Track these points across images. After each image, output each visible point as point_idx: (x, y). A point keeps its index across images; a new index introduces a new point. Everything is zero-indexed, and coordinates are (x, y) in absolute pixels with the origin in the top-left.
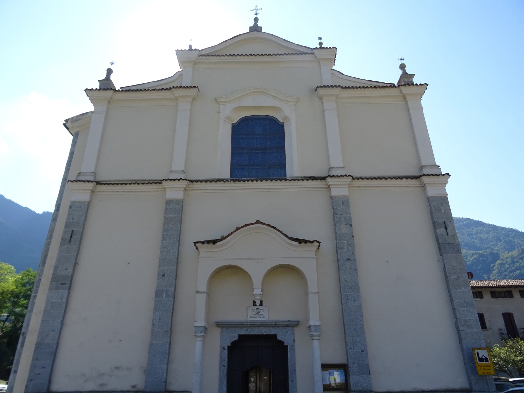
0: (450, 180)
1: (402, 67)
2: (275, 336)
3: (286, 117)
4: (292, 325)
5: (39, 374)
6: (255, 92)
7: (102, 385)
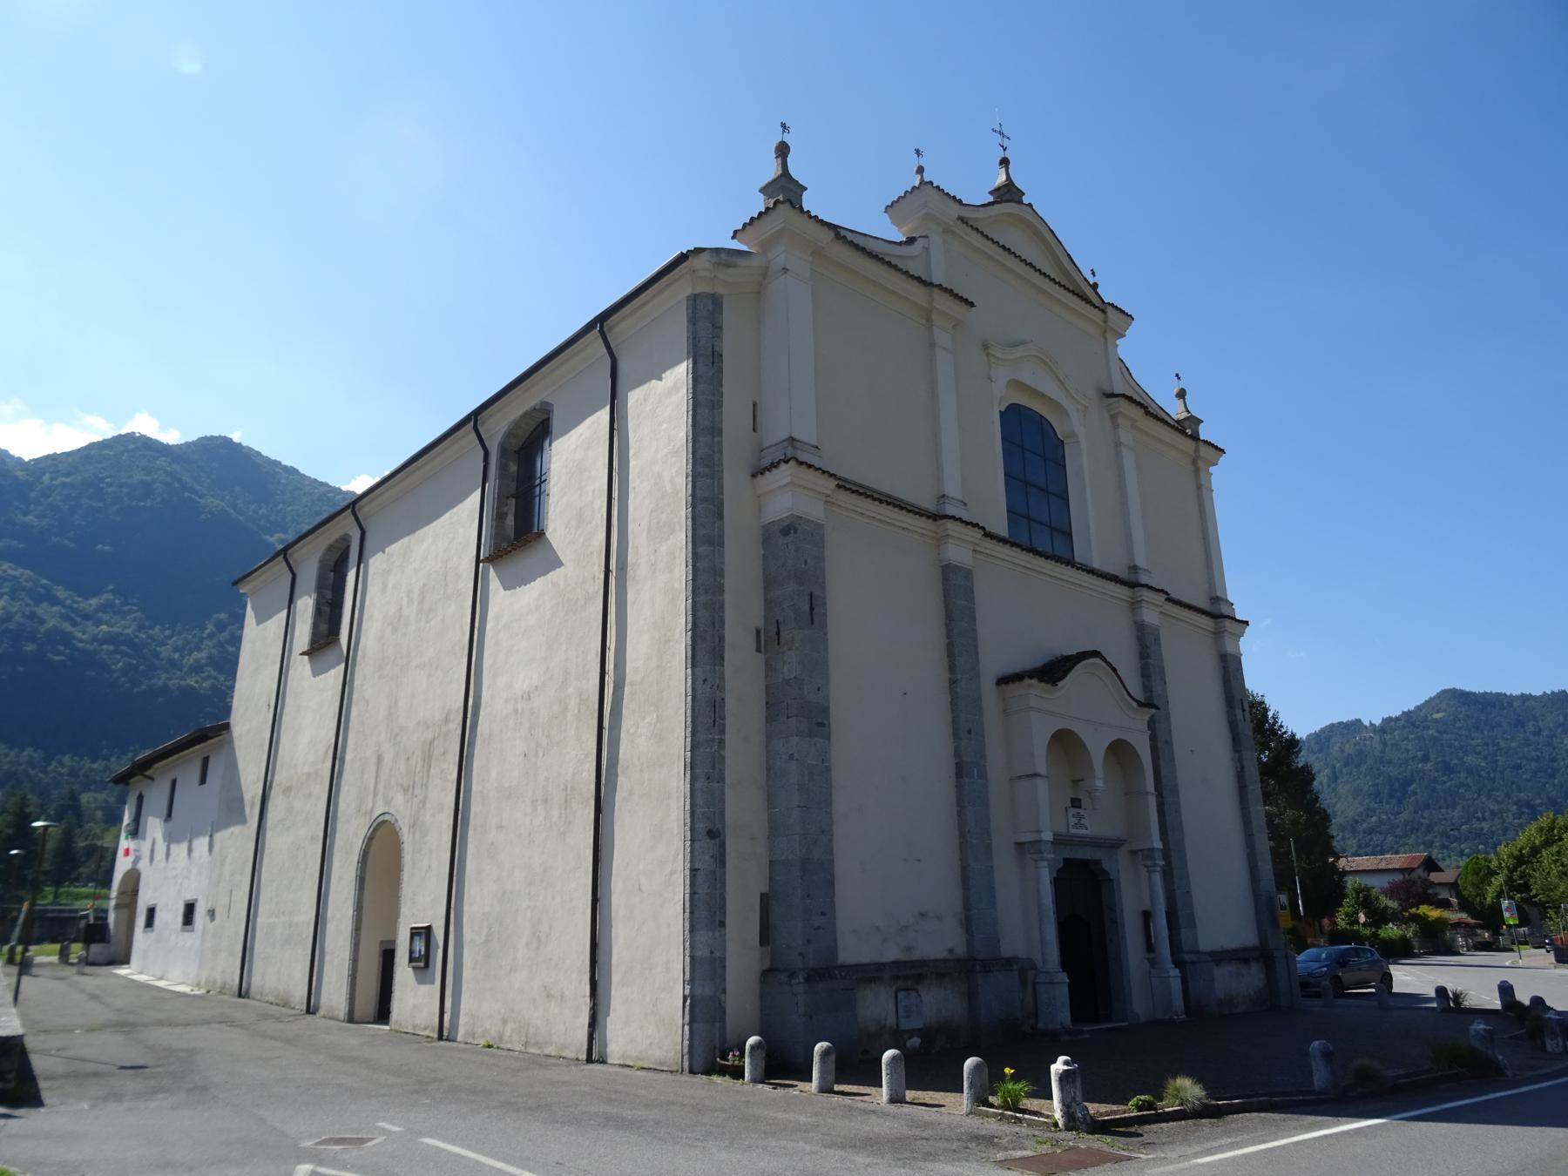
0: (1248, 630)
1: (783, 150)
2: (1098, 862)
3: (1073, 435)
4: (1113, 845)
5: (819, 928)
6: (1041, 359)
7: (908, 949)
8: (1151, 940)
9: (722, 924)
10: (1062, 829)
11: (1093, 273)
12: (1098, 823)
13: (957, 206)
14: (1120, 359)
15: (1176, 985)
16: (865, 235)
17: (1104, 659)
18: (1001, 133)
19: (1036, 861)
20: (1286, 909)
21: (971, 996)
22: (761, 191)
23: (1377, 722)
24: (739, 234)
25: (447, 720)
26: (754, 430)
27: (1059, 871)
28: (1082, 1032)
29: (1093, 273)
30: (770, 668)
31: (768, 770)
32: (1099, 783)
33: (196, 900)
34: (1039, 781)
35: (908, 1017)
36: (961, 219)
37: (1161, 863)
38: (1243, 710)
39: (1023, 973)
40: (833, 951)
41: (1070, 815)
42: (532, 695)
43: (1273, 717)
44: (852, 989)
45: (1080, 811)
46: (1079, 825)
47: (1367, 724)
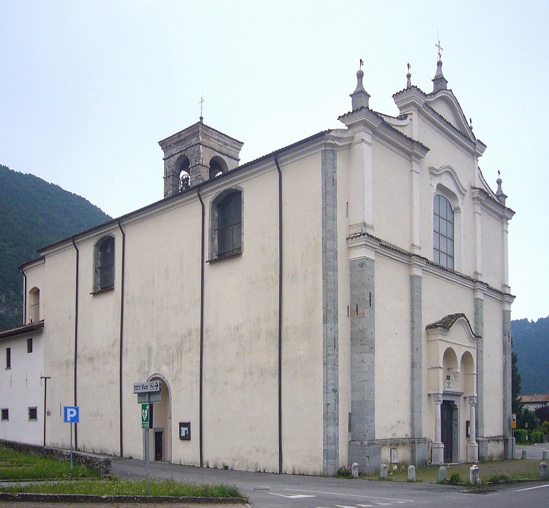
0: (515, 300)
4: (458, 395)
7: (394, 434)
8: (468, 433)
9: (338, 424)
12: (455, 387)
14: (479, 168)
15: (476, 449)
16: (390, 117)
17: (465, 317)
18: (439, 47)
19: (436, 401)
21: (413, 452)
23: (535, 320)
24: (341, 118)
26: (347, 216)
28: (447, 465)
30: (353, 324)
31: (352, 366)
32: (459, 370)
33: (37, 407)
35: (394, 458)
38: (509, 337)
41: (446, 383)
42: (239, 328)
44: (380, 448)
45: (449, 380)
47: (530, 321)
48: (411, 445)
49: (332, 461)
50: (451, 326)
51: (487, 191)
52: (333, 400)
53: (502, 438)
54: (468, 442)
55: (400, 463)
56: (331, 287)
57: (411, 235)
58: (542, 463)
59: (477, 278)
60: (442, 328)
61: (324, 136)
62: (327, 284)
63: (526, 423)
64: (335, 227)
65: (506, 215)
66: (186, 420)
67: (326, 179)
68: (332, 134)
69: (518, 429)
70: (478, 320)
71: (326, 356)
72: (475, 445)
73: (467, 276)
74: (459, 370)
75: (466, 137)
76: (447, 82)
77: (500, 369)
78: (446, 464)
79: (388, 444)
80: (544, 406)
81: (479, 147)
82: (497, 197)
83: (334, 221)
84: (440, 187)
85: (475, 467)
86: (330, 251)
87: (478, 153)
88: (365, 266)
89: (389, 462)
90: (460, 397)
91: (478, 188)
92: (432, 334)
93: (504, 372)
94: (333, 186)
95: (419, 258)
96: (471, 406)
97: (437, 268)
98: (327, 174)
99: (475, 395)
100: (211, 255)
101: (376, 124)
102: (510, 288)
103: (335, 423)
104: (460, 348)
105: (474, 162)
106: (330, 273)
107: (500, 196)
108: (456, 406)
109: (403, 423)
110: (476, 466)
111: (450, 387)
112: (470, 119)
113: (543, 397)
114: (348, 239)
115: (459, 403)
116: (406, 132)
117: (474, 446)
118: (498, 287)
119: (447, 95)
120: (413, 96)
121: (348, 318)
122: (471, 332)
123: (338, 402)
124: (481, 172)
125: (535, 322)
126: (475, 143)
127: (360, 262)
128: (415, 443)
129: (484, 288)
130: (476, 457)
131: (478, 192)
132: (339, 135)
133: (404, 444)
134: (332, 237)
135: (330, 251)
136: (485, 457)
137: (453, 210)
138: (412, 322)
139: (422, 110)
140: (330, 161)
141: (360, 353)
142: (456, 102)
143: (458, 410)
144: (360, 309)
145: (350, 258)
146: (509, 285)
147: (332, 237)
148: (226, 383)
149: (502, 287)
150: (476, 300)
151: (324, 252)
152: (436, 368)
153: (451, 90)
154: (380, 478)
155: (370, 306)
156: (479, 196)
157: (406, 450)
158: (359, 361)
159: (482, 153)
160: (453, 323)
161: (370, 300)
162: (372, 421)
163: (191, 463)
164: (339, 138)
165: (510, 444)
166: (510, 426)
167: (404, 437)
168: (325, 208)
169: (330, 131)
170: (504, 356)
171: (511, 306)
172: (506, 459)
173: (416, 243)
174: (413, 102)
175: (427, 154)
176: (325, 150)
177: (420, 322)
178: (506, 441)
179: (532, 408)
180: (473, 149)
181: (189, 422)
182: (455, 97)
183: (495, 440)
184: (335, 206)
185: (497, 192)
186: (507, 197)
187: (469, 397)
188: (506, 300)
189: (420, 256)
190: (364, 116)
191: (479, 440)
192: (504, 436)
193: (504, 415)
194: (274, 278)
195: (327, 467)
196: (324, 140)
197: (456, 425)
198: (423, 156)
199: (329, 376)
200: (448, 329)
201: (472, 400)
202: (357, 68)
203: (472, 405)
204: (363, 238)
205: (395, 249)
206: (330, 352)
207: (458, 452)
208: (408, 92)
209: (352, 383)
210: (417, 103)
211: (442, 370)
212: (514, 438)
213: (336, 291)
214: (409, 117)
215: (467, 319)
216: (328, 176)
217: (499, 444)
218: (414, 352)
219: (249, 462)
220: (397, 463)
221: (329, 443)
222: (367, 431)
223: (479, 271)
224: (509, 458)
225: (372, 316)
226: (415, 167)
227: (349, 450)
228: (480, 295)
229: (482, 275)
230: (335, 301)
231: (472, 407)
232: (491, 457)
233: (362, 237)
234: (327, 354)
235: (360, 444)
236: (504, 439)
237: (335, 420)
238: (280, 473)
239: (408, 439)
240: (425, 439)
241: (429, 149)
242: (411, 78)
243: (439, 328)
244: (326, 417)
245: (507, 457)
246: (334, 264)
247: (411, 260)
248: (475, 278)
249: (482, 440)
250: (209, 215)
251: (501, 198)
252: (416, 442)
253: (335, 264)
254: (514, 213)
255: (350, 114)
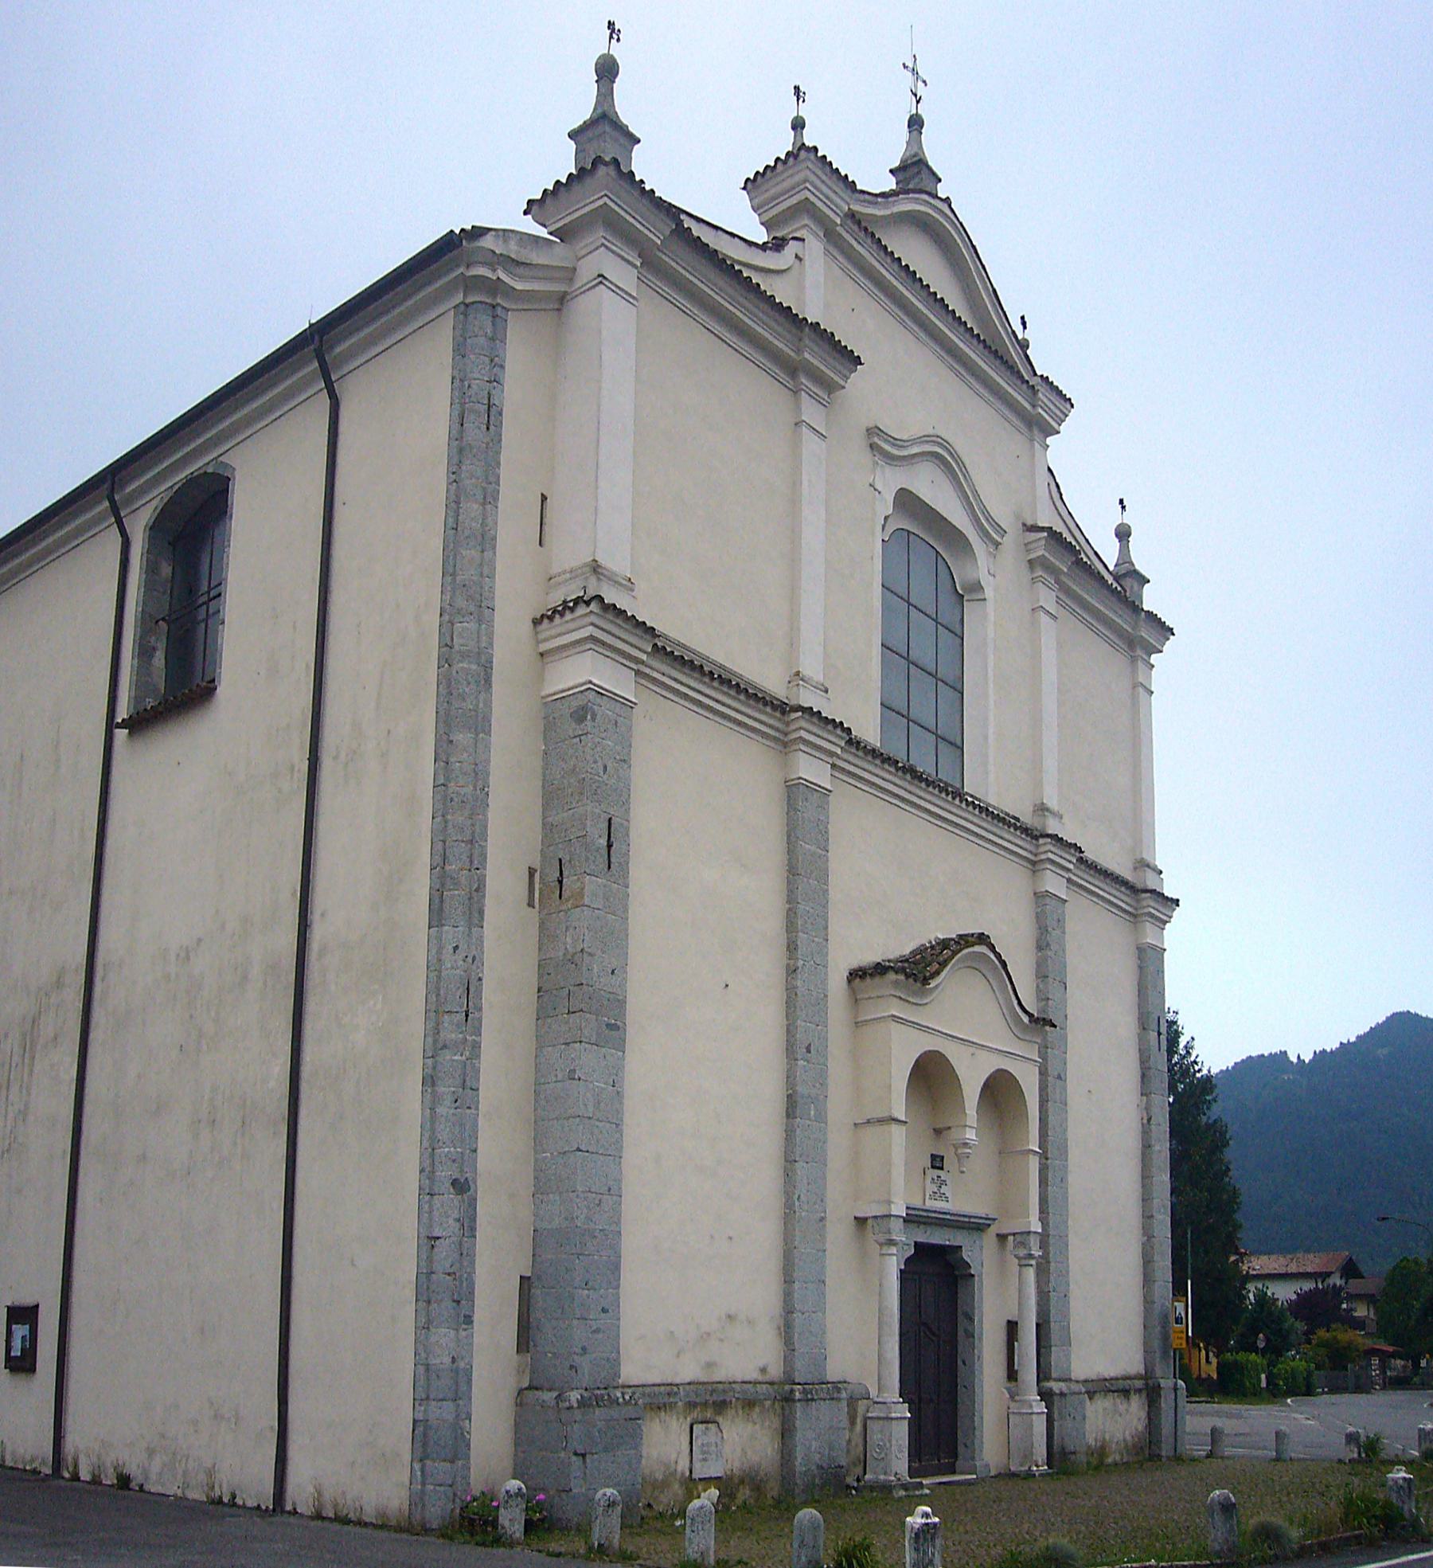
0: (1177, 913)
4: (977, 1226)
7: (710, 1365)
9: (468, 1320)
10: (917, 1202)
11: (1024, 324)
13: (846, 194)
14: (1049, 470)
15: (1040, 1426)
16: (717, 228)
17: (992, 948)
19: (881, 1245)
20: (1182, 1323)
21: (786, 1432)
22: (572, 135)
23: (1307, 1057)
24: (535, 208)
25: (59, 984)
26: (540, 544)
27: (908, 1261)
29: (1024, 324)
30: (546, 934)
32: (971, 1135)
34: (895, 1129)
35: (705, 1460)
36: (852, 215)
37: (1037, 1253)
39: (852, 1402)
40: (615, 1363)
41: (929, 1180)
42: (192, 955)
43: (1186, 1047)
45: (940, 1172)
46: (939, 1195)
48: (779, 1411)
49: (440, 1469)
50: (937, 973)
51: (1074, 543)
52: (451, 1221)
53: (1139, 1384)
54: (1012, 1397)
55: (730, 1478)
56: (463, 791)
57: (793, 644)
58: (1217, 1492)
59: (1044, 825)
60: (902, 977)
61: (460, 249)
62: (447, 778)
63: (1261, 1335)
64: (486, 571)
65: (1143, 635)
66: (27, 1300)
67: (463, 404)
68: (487, 242)
69: (1237, 1353)
70: (1048, 970)
71: (435, 1048)
72: (1036, 1410)
73: (1008, 815)
74: (971, 1135)
75: (1002, 358)
76: (940, 180)
77: (1131, 1141)
78: (918, 1480)
79: (680, 1404)
80: (1320, 1287)
81: (1045, 400)
82: (1117, 578)
83: (483, 551)
84: (906, 501)
85: (926, 1515)
86: (464, 656)
87: (1051, 426)
88: (593, 719)
89: (683, 1474)
90: (985, 1237)
91: (1042, 529)
92: (870, 998)
93: (1143, 1154)
94: (488, 429)
95: (815, 720)
96: (1020, 1266)
97: (892, 770)
98: (469, 386)
99: (1033, 1229)
100: (137, 699)
101: (656, 233)
102: (1161, 872)
103: (458, 1315)
104: (973, 1054)
105: (1033, 446)
106: (462, 737)
107: (1125, 575)
108: (970, 1267)
109: (750, 1322)
110: (928, 1510)
111: (943, 1197)
112: (1023, 318)
113: (1317, 1261)
114: (536, 622)
115: (980, 1255)
116: (781, 291)
117: (1032, 1414)
118: (1118, 864)
119: (930, 211)
120: (805, 181)
121: (531, 909)
122: (1015, 1002)
123: (473, 1229)
124: (1058, 486)
125: (1307, 1061)
126: (1033, 386)
127: (575, 704)
128: (794, 1401)
129: (1069, 860)
130: (1040, 1452)
131: (1043, 542)
132: (513, 249)
133: (749, 1404)
134: (472, 608)
135: (464, 656)
136: (1074, 1453)
137: (960, 592)
138: (792, 947)
139: (840, 235)
140: (482, 340)
141: (567, 1044)
142: (963, 241)
143: (976, 1278)
144: (571, 878)
145: (543, 694)
146: (1157, 863)
147: (472, 608)
148: (143, 1158)
149: (1135, 869)
150: (1041, 897)
151: (445, 660)
152: (881, 1121)
153: (947, 201)
154: (590, 1549)
155: (609, 867)
156: (1047, 554)
157: (757, 1426)
158: (560, 1077)
159: (1060, 425)
160: (943, 964)
161: (610, 846)
162: (604, 1310)
163: (33, 1460)
164: (513, 260)
165: (1166, 1404)
166: (1165, 1337)
167: (753, 1375)
168: (454, 504)
169: (478, 232)
170: (1145, 1098)
171: (1165, 931)
172: (1155, 1457)
173: (812, 668)
174: (1043, 555)
175: (853, 375)
176: (467, 305)
177: (823, 951)
178: (1152, 1393)
179: (1284, 1293)
180: (1029, 407)
181: (36, 1303)
182: (961, 224)
183: (1113, 1392)
184: (490, 498)
185: (1116, 566)
186: (1148, 581)
187: (1014, 1234)
188: (1146, 910)
189: (819, 712)
190: (603, 193)
191: (1051, 1389)
192: (1148, 1375)
193: (1148, 1301)
194: (296, 769)
195: (423, 1492)
196: (458, 266)
197: (970, 1335)
198: (842, 383)
199: (442, 1127)
200: (925, 981)
201: (1023, 1244)
202: (599, 45)
203: (1024, 1262)
204: (586, 615)
205: (720, 676)
206: (449, 1034)
207: (977, 1433)
208: (791, 167)
209: (536, 1160)
210: (819, 204)
211: (904, 1128)
212: (1180, 1382)
213: (479, 803)
214: (792, 248)
215: (998, 956)
216: (472, 392)
217: (1129, 1404)
218: (796, 1060)
219: (191, 1460)
220: (718, 1478)
221: (431, 1397)
222: (584, 1349)
223: (1052, 803)
224: (1164, 1453)
225: (618, 906)
226: (810, 412)
227: (516, 1424)
228: (1053, 883)
229: (1061, 818)
230: (475, 841)
231: (1024, 1269)
232: (1102, 1450)
233: (582, 610)
234: (435, 1042)
235: (553, 1403)
236: (1147, 1384)
237: (458, 1302)
238: (274, 1510)
239: (772, 1383)
240: (837, 1386)
241: (859, 357)
242: (804, 131)
243: (892, 976)
244: (425, 1293)
245: (1158, 1452)
246: (477, 706)
247: (788, 724)
248: (1036, 825)
249: (1065, 1390)
250: (141, 568)
251: (1128, 583)
252: (798, 1395)
253: (481, 705)
254: (1171, 631)
255: (562, 189)
